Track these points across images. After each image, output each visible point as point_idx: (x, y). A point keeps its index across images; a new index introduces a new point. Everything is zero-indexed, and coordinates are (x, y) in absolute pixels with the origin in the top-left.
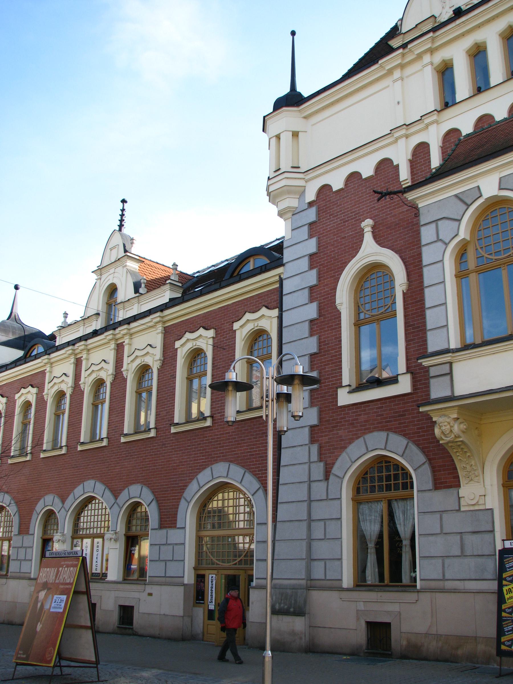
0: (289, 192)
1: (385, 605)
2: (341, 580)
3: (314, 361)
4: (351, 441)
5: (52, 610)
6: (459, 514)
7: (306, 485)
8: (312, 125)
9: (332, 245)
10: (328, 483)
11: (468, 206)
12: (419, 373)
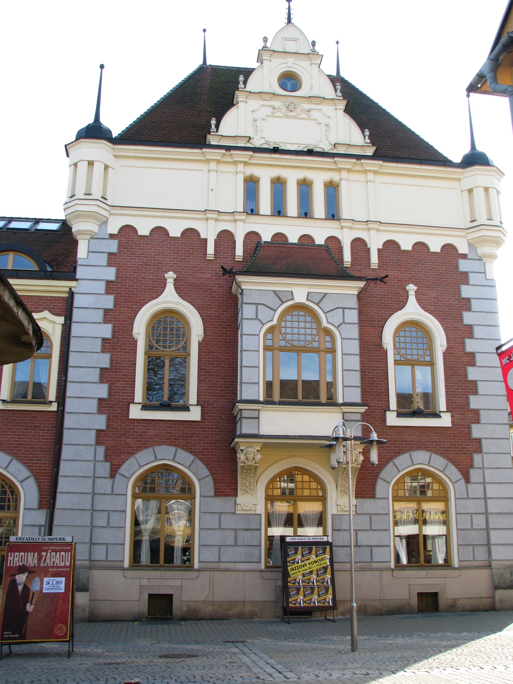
0: (95, 218)
1: (164, 581)
2: (123, 561)
3: (104, 375)
4: (139, 449)
5: (44, 591)
6: (235, 516)
7: (91, 481)
8: (121, 166)
9: (132, 280)
10: (114, 480)
11: (283, 303)
12: (207, 407)
